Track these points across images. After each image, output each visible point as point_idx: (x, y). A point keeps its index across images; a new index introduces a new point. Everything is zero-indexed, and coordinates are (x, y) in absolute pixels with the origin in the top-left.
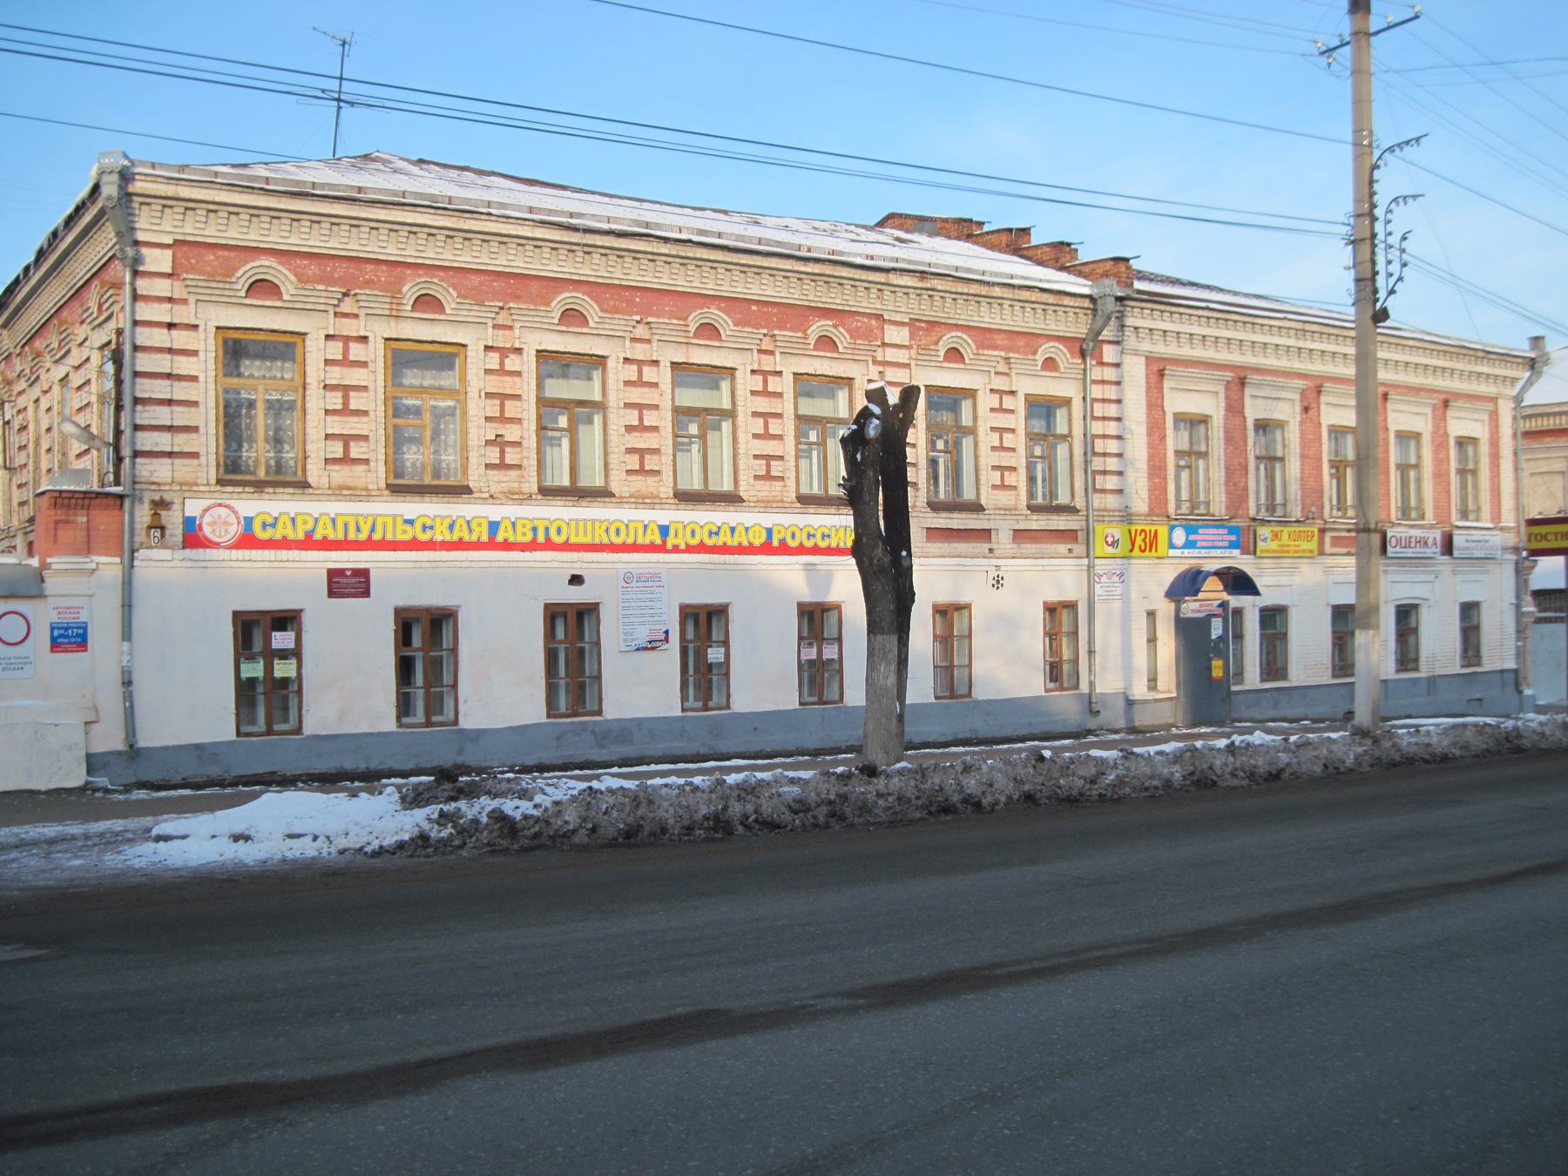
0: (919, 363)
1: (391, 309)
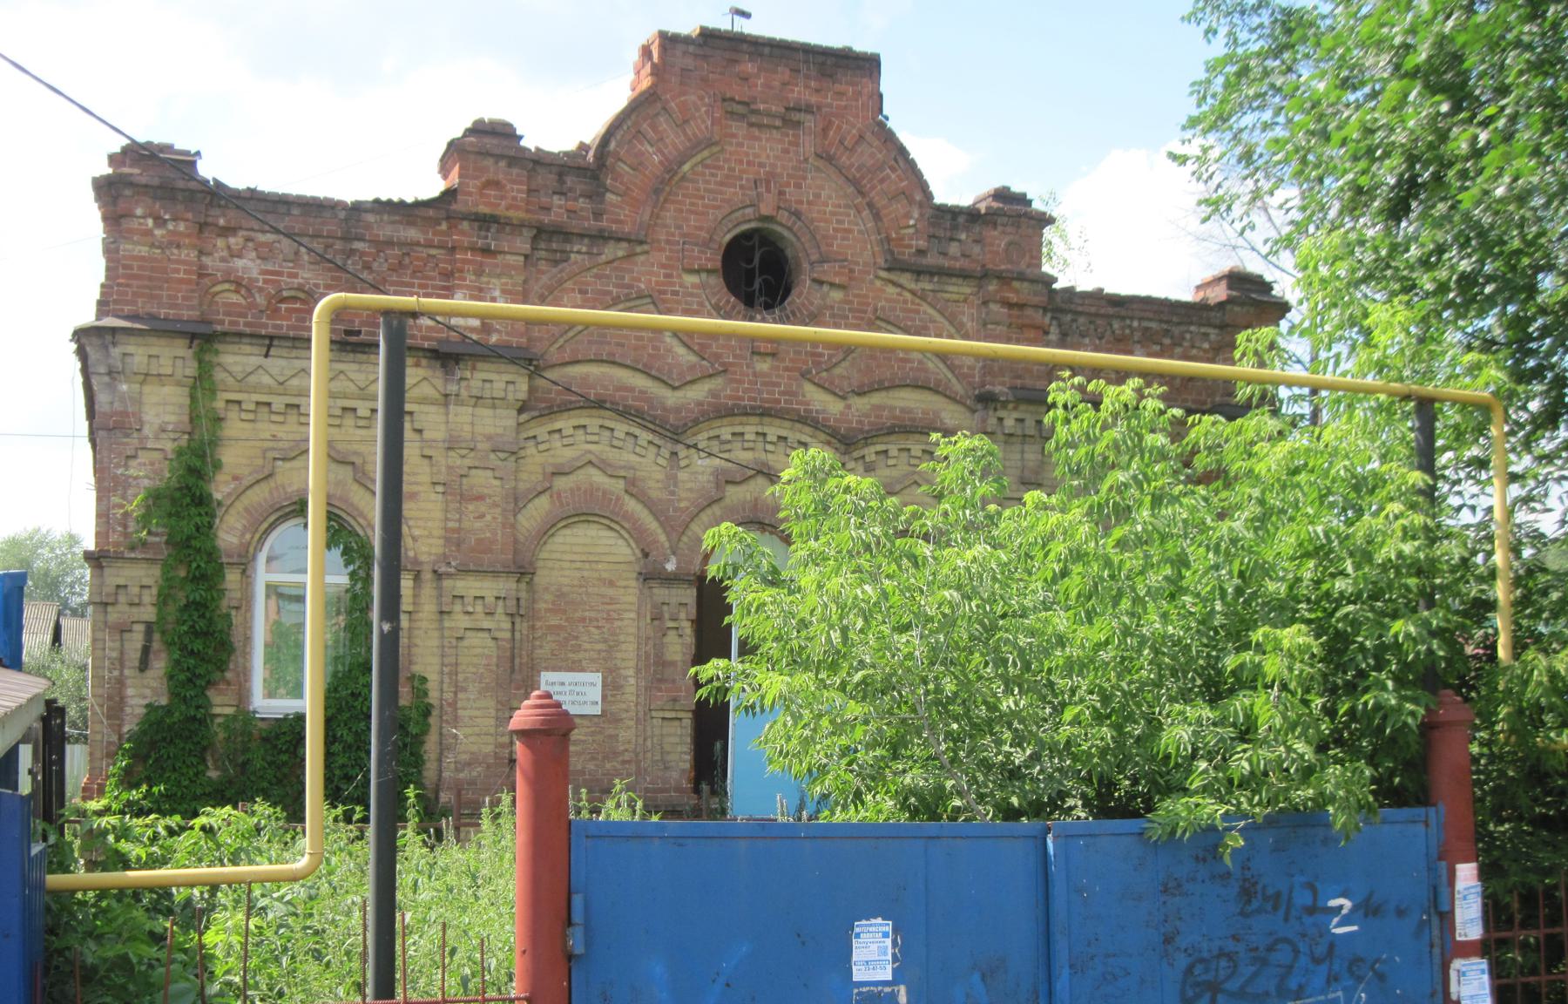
1: (562, 569)
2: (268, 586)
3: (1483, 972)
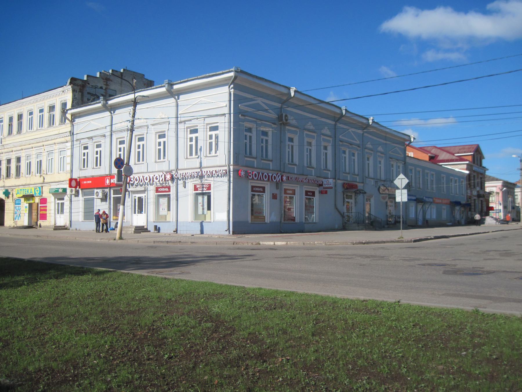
0: (13, 171)
2: (276, 199)
3: (227, 182)
